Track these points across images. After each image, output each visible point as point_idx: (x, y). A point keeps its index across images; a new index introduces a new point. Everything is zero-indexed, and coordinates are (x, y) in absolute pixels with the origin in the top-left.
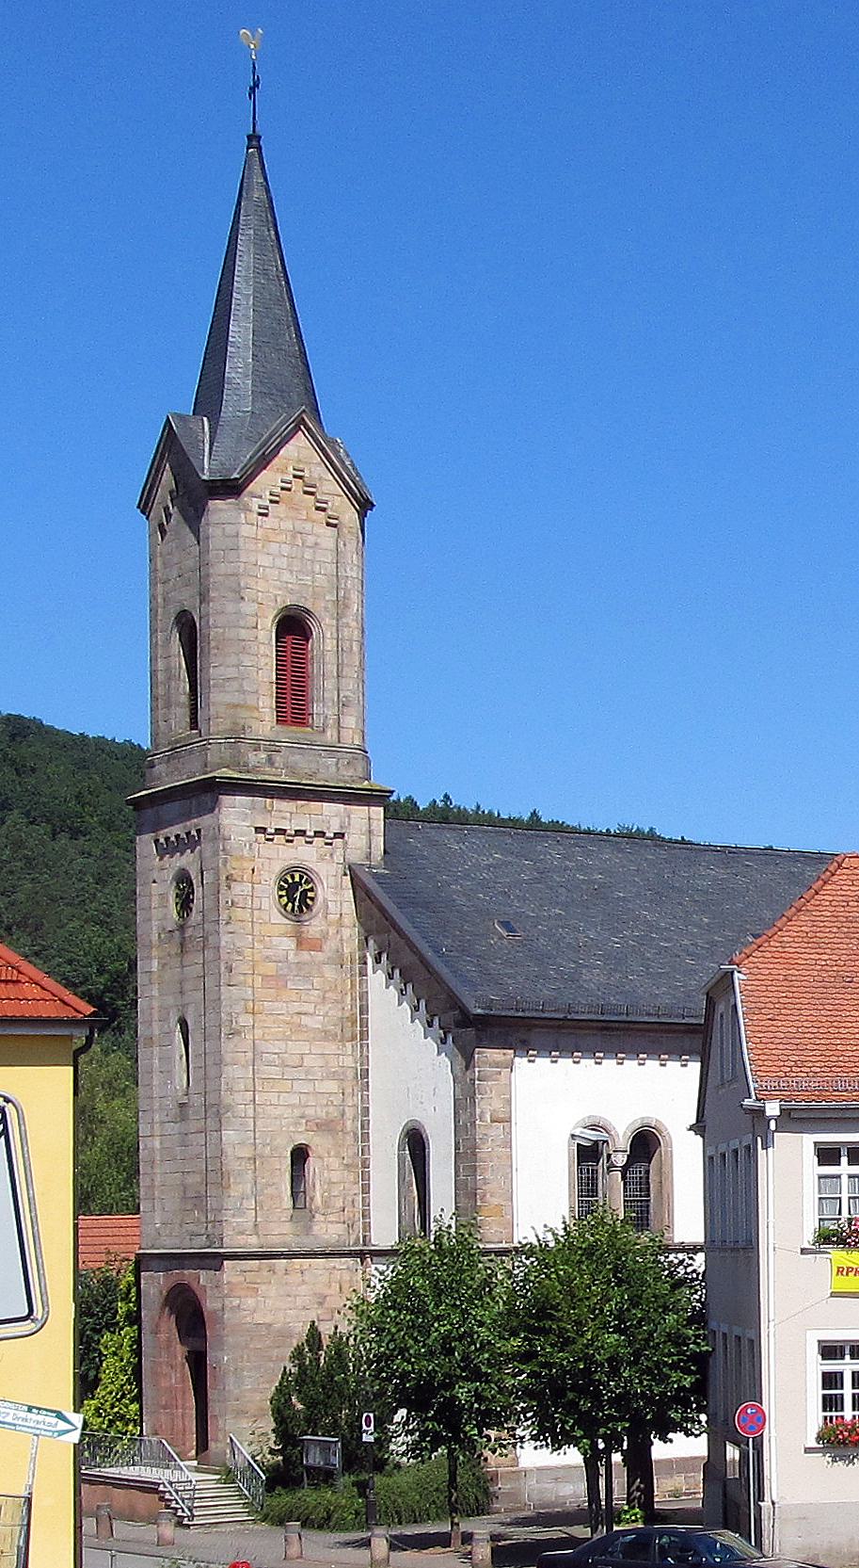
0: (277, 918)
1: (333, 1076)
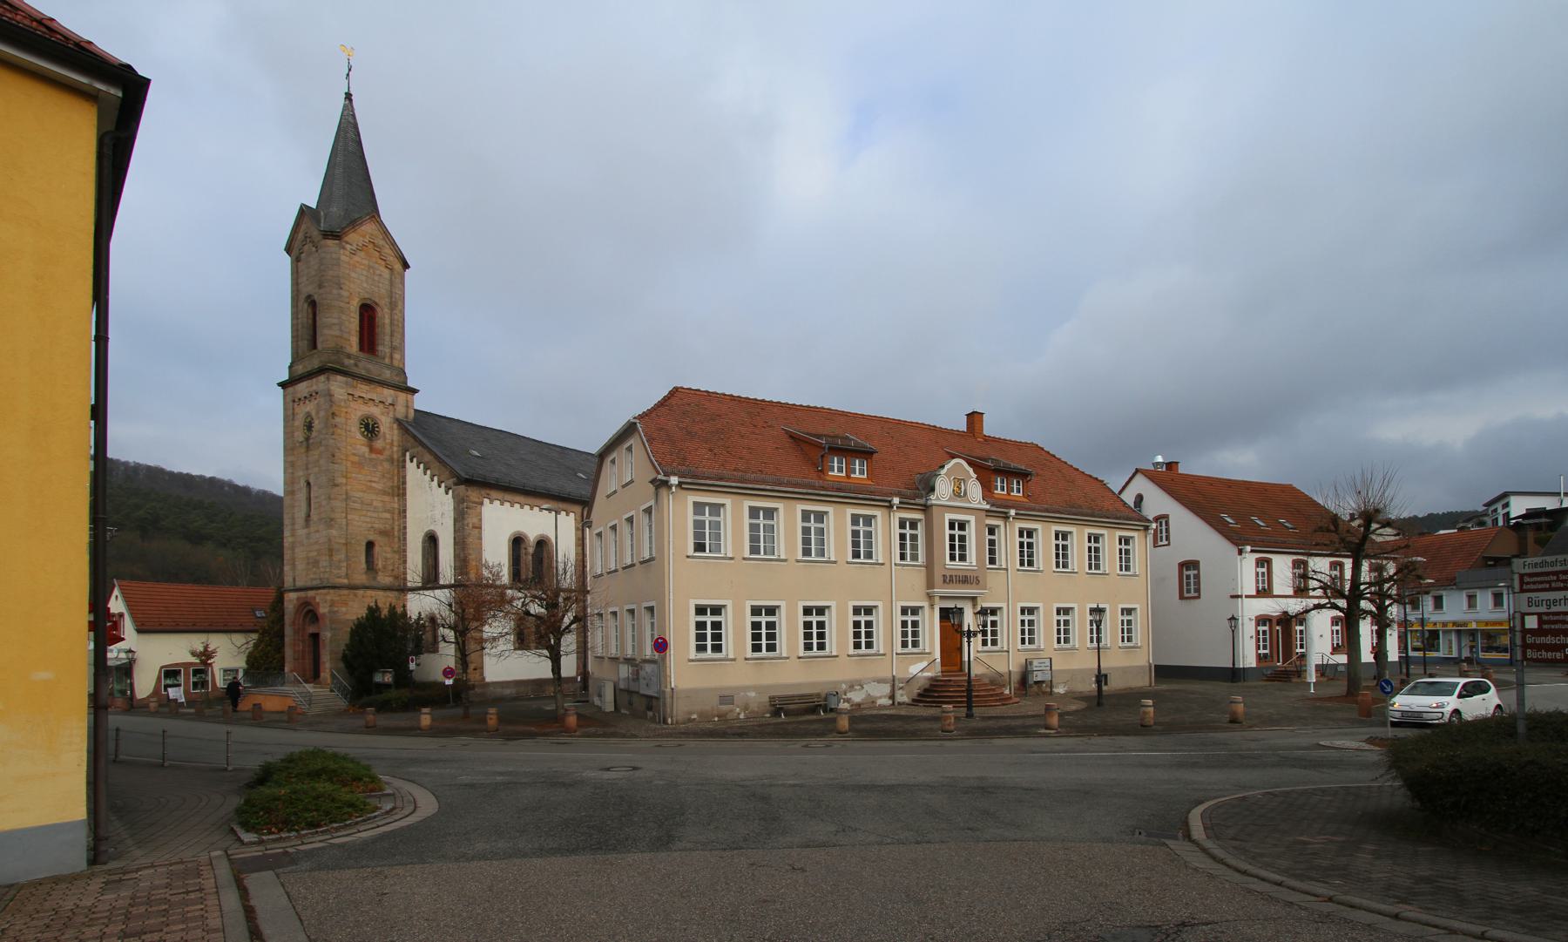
0: (359, 436)
1: (388, 511)
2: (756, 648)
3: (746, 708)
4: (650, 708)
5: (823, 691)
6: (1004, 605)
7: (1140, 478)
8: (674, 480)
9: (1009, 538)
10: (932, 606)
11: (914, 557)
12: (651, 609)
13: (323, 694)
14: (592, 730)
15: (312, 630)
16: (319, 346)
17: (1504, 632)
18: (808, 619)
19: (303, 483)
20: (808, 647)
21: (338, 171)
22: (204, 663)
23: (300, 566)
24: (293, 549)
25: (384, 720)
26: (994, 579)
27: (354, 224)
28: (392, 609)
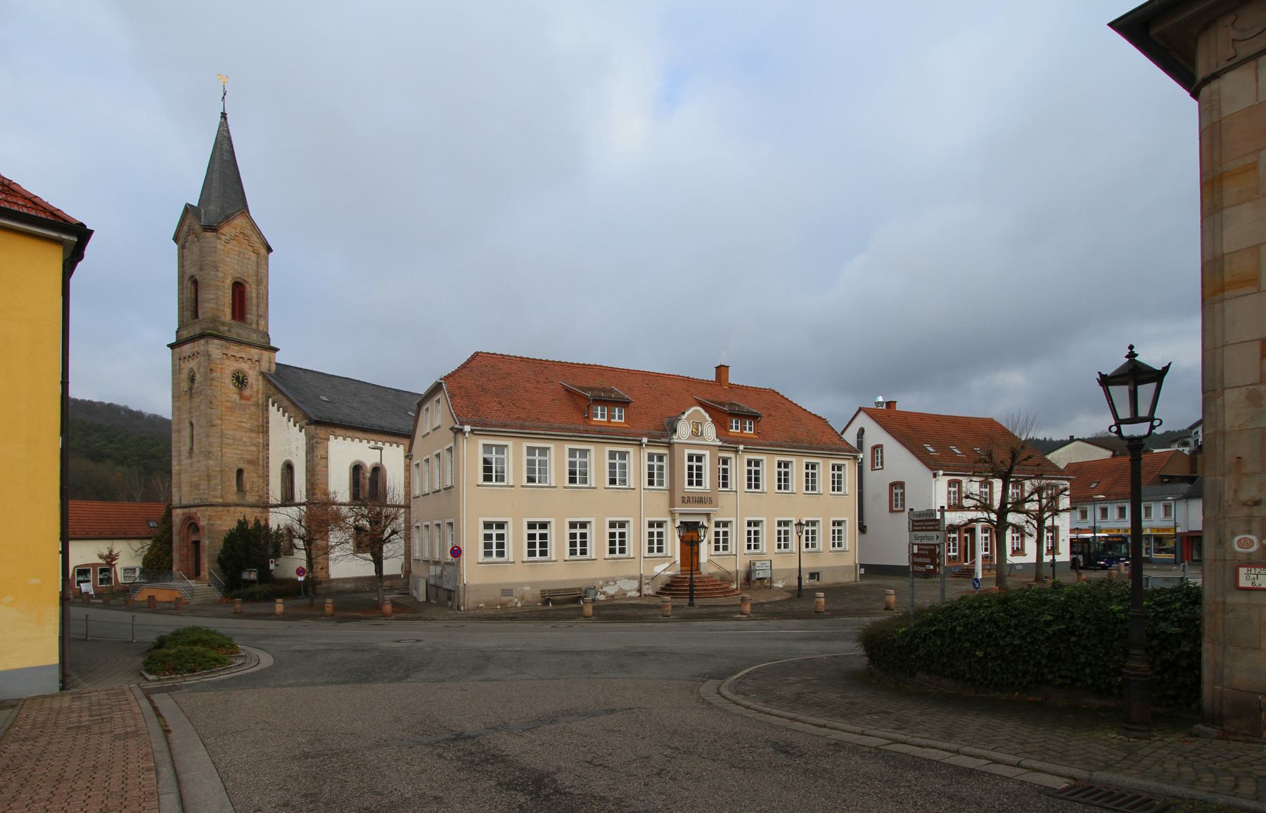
2: (532, 554)
3: (522, 599)
4: (449, 599)
5: (583, 586)
6: (734, 519)
7: (862, 415)
8: (467, 428)
9: (738, 468)
10: (674, 520)
11: (661, 483)
12: (451, 524)
13: (203, 588)
14: (404, 615)
15: (194, 538)
16: (200, 316)
17: (1169, 537)
18: (573, 531)
19: (187, 424)
20: (573, 552)
21: (216, 176)
22: (109, 564)
23: (185, 488)
24: (179, 474)
25: (249, 608)
26: (725, 499)
27: (227, 218)
28: (257, 522)
